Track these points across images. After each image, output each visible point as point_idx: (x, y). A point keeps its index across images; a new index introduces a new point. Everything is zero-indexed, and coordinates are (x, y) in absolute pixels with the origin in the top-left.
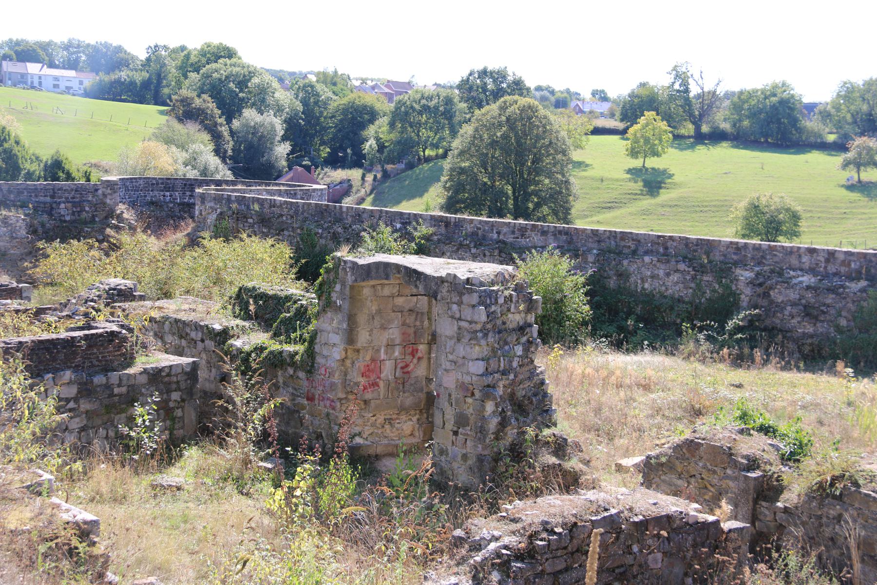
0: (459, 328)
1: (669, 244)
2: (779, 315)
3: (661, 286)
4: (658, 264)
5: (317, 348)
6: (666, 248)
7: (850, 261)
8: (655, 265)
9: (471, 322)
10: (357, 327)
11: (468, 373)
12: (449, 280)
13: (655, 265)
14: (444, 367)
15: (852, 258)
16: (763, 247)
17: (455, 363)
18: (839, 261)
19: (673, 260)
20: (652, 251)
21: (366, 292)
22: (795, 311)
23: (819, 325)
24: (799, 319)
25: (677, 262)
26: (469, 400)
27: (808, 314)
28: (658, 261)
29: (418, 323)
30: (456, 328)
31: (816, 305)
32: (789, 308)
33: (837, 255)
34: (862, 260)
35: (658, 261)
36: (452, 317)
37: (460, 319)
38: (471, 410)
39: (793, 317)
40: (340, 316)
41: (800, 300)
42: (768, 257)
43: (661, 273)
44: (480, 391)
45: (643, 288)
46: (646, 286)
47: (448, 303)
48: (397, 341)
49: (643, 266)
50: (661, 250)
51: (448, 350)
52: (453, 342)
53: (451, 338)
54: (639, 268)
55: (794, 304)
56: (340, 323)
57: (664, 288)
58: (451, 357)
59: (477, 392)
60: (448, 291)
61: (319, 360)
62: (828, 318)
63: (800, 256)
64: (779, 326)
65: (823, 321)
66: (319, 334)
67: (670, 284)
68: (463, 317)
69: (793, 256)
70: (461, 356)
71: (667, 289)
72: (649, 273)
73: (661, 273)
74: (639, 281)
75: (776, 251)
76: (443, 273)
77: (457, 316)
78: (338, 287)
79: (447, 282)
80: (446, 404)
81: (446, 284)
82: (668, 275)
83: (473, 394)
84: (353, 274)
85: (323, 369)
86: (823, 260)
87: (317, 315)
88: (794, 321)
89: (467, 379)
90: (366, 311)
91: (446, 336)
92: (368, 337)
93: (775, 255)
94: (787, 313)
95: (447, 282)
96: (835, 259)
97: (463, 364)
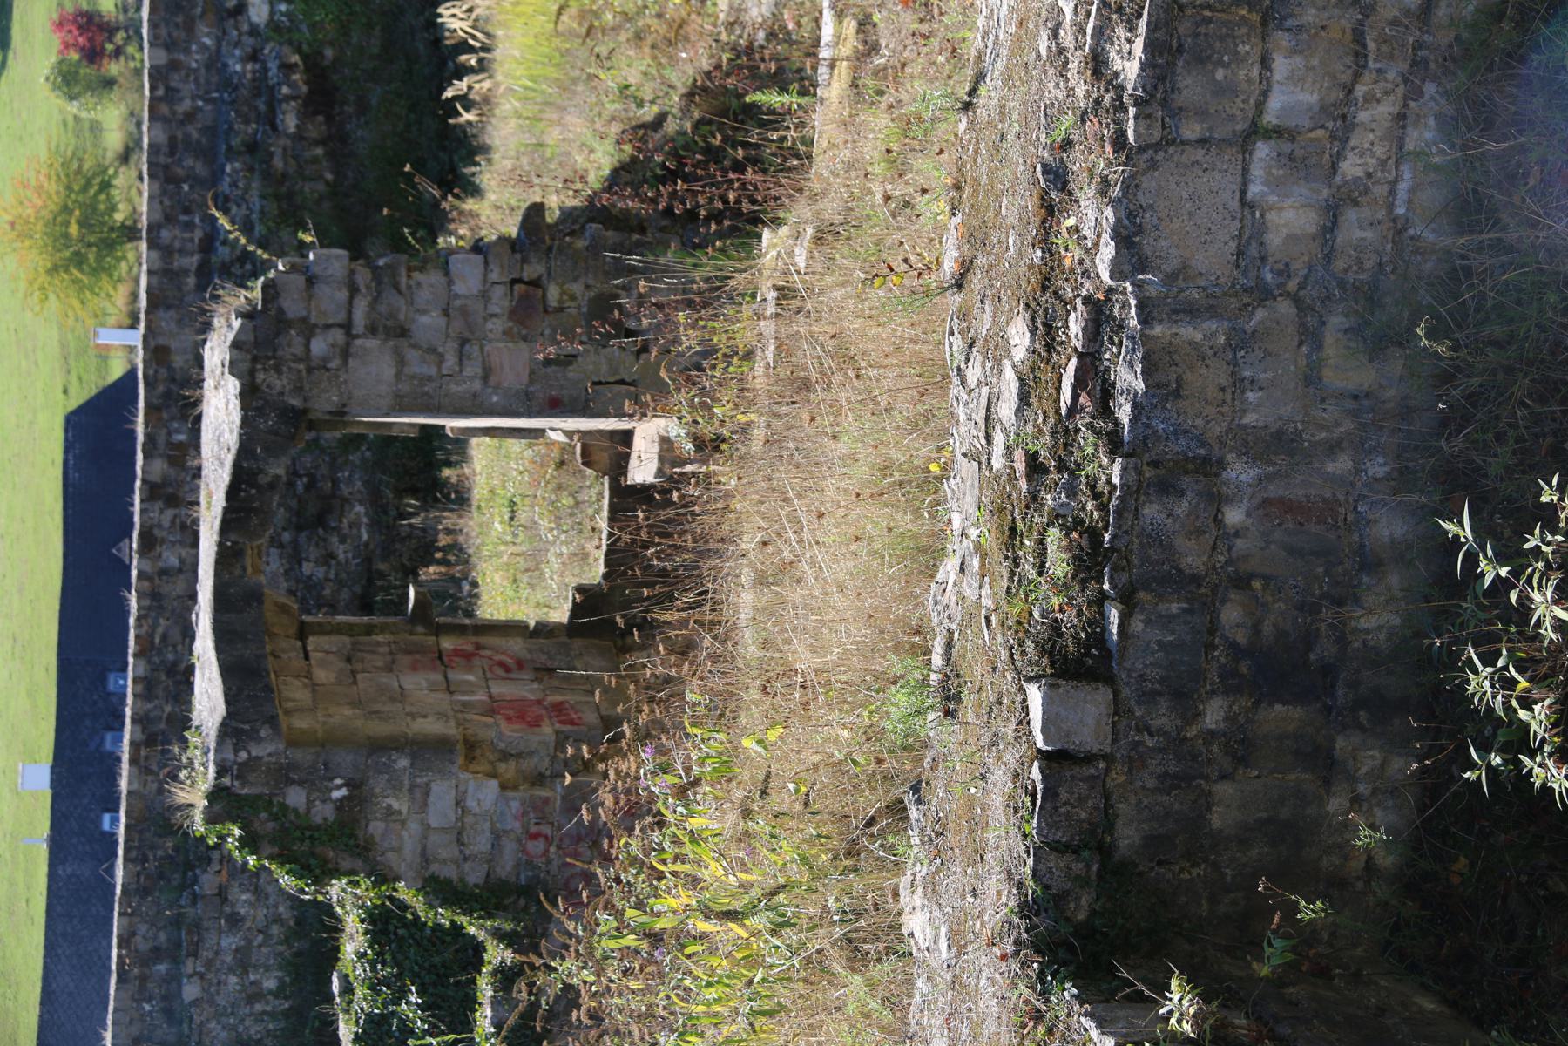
0: (372, 330)
1: (141, 944)
2: (327, 592)
3: (268, 937)
4: (206, 954)
5: (475, 876)
6: (157, 953)
7: (172, 445)
8: (209, 964)
9: (354, 290)
10: (405, 736)
11: (485, 296)
12: (246, 366)
13: (209, 964)
14: (477, 385)
15: (161, 440)
16: (141, 672)
17: (464, 342)
18: (172, 472)
19: (190, 911)
20: (164, 998)
21: (301, 723)
22: (314, 553)
23: (345, 490)
24: (335, 539)
25: (195, 898)
26: (553, 293)
27: (320, 520)
28: (195, 955)
29: (381, 650)
30: (372, 343)
31: (294, 503)
32: (307, 568)
33: (155, 477)
34: (165, 416)
35: (195, 955)
36: (345, 353)
37: (347, 327)
38: (576, 288)
39: (332, 556)
40: (378, 784)
41: (281, 546)
42: (170, 657)
43: (230, 942)
44: (524, 261)
45: (276, 994)
46: (270, 984)
47: (309, 370)
48: (437, 677)
49: (212, 1002)
50: (162, 968)
51: (433, 371)
52: (412, 355)
53: (401, 362)
54: (219, 1015)
55: (296, 558)
56: (395, 786)
57: (275, 930)
58: (451, 361)
59: (529, 272)
60: (277, 369)
61: (506, 867)
62: (324, 470)
63: (164, 572)
64: (358, 589)
65: (335, 482)
66: (435, 868)
67: (261, 912)
68: (341, 317)
69: (166, 589)
70: (442, 321)
71: (278, 920)
72: (233, 980)
73: (230, 942)
74: (258, 1007)
75: (151, 635)
76: (233, 385)
77: (338, 336)
78: (296, 797)
79: (252, 373)
80: (572, 373)
81: (260, 376)
82: (235, 921)
83: (535, 283)
84: (253, 736)
85: (530, 845)
86: (170, 513)
87: (383, 878)
88: (341, 551)
89: (500, 301)
90: (359, 723)
91: (398, 375)
92: (430, 719)
93: (164, 637)
94: (320, 573)
95: (252, 373)
96: (166, 482)
97: (464, 312)
